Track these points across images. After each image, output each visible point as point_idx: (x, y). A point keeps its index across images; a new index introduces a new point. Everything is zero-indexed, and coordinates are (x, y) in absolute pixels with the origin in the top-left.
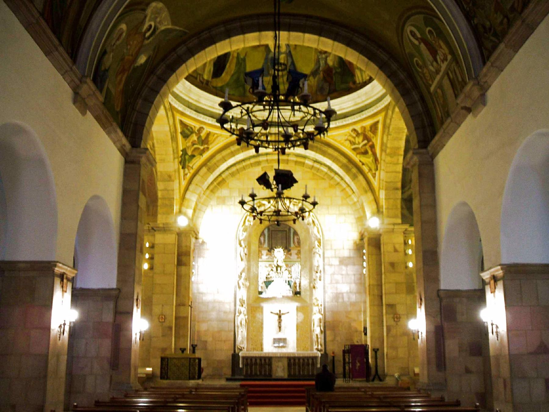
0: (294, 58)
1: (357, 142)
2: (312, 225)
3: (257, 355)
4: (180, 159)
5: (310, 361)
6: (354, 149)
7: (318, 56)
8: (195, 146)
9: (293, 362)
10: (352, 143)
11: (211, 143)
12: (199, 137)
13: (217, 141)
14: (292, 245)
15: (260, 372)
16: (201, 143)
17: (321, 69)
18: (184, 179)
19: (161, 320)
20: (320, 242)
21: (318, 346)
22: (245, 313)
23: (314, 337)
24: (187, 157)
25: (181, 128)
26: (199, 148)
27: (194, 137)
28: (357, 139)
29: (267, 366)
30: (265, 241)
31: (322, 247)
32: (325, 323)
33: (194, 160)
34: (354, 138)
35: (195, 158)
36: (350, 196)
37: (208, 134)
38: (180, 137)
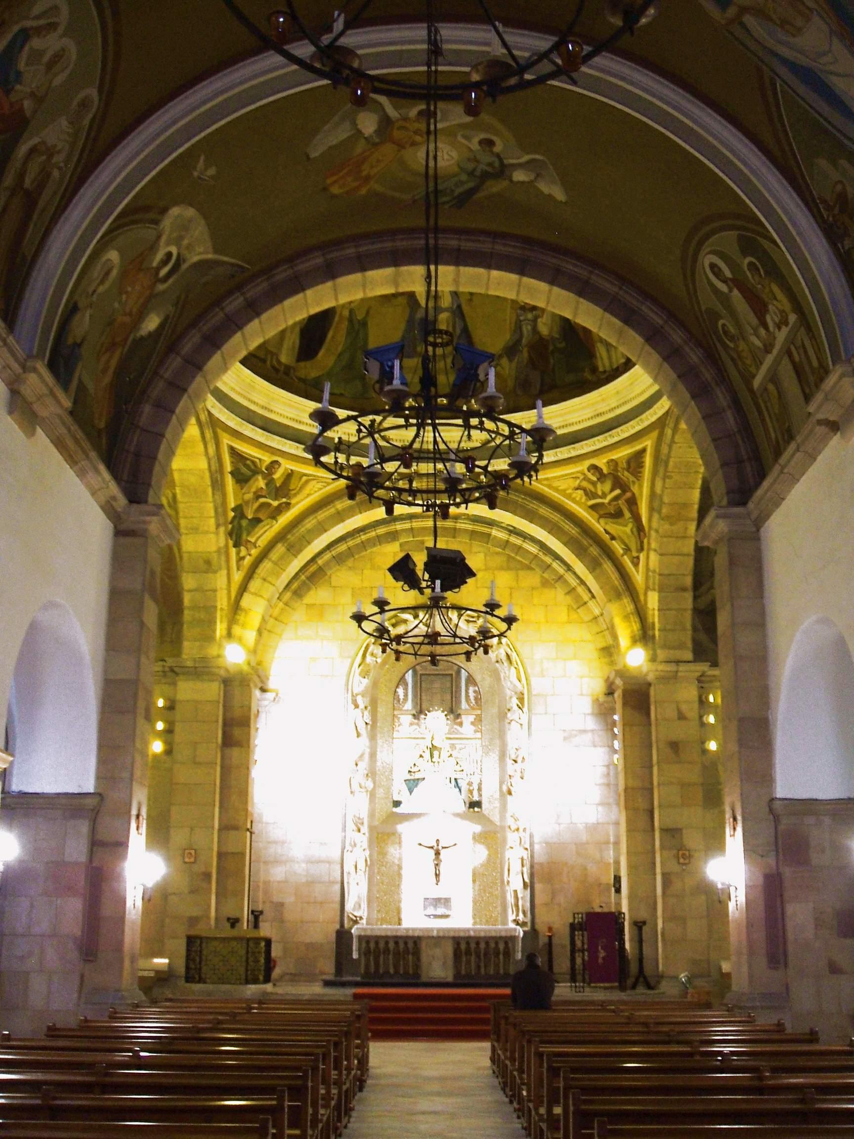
0: (468, 320)
1: (600, 493)
2: (506, 664)
3: (389, 934)
4: (230, 526)
5: (501, 946)
6: (593, 507)
7: (518, 316)
8: (262, 500)
9: (464, 947)
10: (590, 495)
11: (295, 495)
12: (270, 482)
13: (307, 490)
14: (464, 705)
15: (396, 967)
16: (273, 494)
17: (524, 341)
18: (238, 569)
19: (187, 860)
20: (521, 699)
21: (517, 915)
22: (365, 845)
23: (510, 899)
24: (244, 523)
25: (232, 462)
26: (269, 505)
27: (261, 483)
28: (599, 485)
29: (410, 957)
30: (406, 695)
31: (525, 709)
32: (532, 867)
33: (259, 530)
34: (594, 484)
35: (261, 525)
36: (585, 603)
37: (289, 475)
38: (229, 481)
